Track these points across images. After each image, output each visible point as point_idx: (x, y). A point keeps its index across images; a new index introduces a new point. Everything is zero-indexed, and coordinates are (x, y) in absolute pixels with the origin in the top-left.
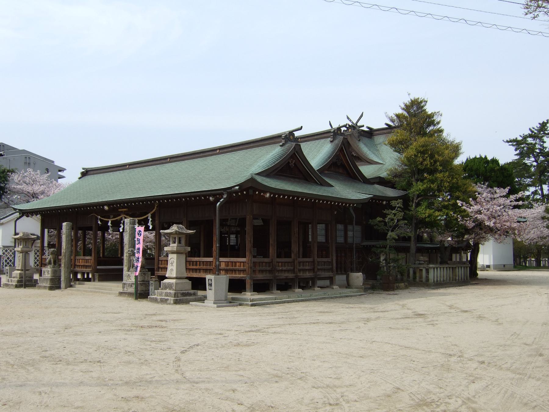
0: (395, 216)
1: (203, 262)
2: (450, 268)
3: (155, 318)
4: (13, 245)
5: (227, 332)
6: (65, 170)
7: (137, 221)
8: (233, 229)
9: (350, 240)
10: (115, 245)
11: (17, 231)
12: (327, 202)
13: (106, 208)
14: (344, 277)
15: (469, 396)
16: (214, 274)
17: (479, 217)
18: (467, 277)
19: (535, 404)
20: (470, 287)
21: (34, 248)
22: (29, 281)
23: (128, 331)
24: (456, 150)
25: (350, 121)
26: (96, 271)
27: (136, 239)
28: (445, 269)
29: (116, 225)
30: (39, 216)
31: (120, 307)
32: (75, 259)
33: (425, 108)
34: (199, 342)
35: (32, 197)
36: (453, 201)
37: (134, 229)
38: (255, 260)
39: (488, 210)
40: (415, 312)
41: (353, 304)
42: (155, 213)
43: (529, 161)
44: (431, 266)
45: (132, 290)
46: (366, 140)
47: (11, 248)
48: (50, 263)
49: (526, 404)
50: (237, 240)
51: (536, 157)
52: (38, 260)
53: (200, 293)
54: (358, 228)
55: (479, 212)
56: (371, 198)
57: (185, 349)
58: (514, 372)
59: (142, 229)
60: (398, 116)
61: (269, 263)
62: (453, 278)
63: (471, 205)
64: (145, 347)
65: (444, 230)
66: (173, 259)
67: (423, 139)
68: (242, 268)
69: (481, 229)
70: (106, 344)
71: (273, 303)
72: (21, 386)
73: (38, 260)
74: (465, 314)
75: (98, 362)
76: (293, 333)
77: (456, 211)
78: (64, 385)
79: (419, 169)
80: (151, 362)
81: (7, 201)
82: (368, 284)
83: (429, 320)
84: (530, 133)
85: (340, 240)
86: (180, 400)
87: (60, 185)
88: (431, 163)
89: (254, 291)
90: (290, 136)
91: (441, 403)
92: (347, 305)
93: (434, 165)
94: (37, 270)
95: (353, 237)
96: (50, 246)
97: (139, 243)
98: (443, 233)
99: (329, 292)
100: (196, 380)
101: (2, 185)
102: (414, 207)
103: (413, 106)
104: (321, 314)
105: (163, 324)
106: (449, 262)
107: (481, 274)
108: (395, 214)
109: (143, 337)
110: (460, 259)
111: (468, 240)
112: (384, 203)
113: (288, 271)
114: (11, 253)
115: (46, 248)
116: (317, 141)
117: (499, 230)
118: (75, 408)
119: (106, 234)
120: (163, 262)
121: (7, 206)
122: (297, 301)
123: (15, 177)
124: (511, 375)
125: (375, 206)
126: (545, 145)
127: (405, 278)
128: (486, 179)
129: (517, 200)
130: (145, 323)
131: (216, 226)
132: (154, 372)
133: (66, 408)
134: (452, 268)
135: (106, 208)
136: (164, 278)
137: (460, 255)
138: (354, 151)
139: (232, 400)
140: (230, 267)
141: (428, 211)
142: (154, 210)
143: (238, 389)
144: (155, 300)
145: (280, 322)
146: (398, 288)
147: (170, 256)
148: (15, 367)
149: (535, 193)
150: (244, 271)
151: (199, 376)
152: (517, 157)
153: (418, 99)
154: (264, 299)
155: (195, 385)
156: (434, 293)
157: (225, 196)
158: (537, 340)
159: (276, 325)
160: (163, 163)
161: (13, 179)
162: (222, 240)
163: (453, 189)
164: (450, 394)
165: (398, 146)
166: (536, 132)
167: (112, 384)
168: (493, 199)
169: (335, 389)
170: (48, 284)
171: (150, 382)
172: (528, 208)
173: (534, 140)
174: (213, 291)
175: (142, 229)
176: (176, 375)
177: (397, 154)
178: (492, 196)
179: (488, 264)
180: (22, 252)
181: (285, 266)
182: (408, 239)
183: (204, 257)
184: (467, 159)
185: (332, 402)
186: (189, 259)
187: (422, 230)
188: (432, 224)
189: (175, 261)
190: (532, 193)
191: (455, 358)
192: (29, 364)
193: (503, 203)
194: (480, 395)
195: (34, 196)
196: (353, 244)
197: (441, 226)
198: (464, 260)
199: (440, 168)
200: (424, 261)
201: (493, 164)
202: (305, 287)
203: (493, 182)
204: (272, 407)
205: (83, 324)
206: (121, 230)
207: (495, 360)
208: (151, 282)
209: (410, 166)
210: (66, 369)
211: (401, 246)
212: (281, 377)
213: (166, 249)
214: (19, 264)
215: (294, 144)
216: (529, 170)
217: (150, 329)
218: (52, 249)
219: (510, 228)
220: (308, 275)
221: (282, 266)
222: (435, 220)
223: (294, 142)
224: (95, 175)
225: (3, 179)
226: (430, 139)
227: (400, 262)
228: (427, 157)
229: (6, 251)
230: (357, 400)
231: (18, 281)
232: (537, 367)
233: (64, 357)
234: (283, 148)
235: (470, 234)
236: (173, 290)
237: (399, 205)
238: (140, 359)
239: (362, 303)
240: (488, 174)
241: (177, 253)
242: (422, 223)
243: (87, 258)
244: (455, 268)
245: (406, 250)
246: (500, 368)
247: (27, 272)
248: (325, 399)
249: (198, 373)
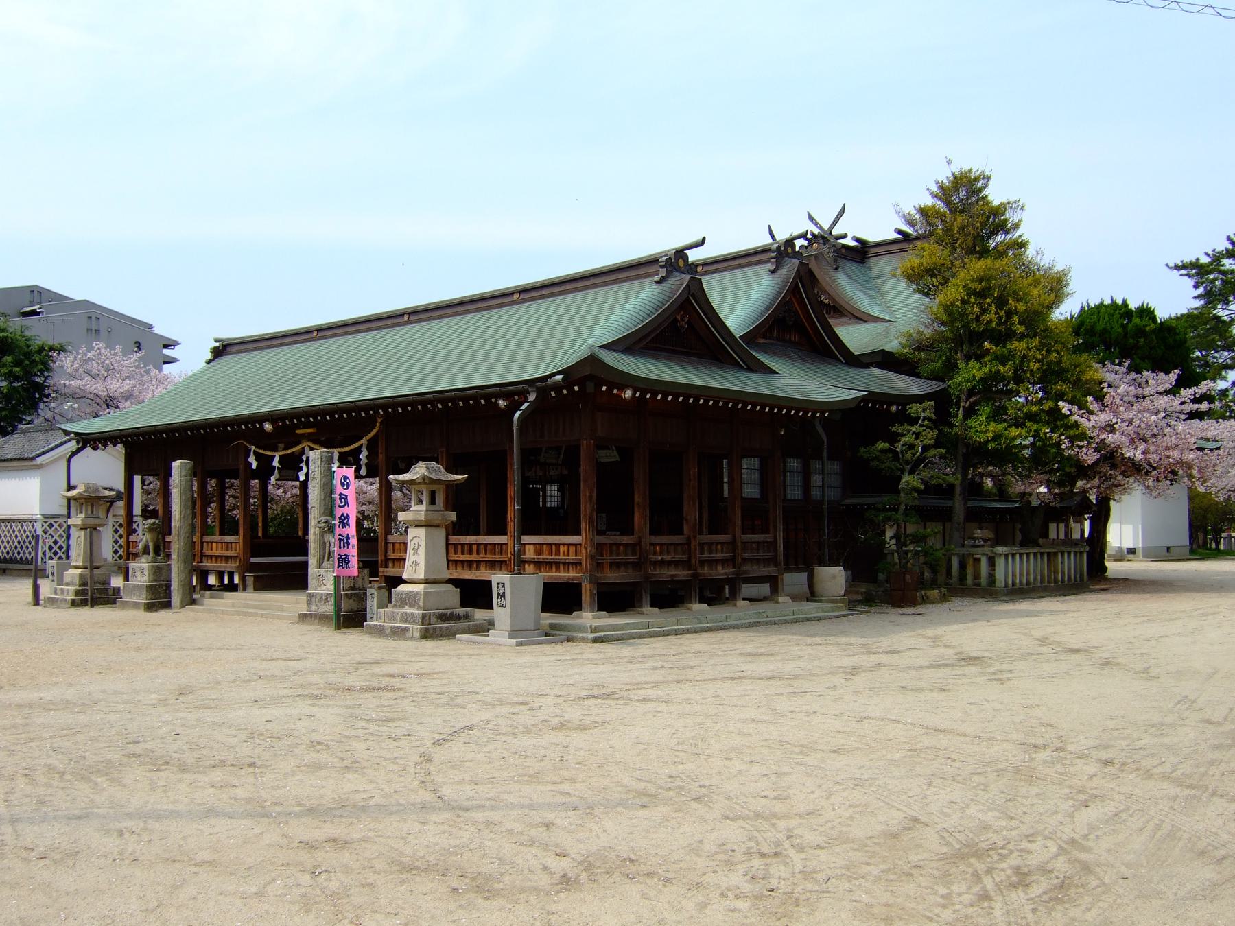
0: (916, 438)
1: (486, 545)
2: (1042, 554)
3: (378, 670)
4: (65, 512)
6: (178, 343)
7: (336, 456)
8: (552, 472)
9: (815, 494)
10: (291, 511)
11: (72, 483)
12: (763, 407)
13: (268, 427)
14: (804, 575)
15: (1076, 836)
16: (510, 571)
17: (1111, 439)
18: (1081, 575)
19: (1223, 852)
20: (1088, 596)
21: (111, 520)
22: (100, 591)
23: (318, 697)
24: (1056, 286)
25: (816, 224)
26: (248, 567)
27: (336, 496)
28: (1032, 557)
29: (292, 465)
30: (120, 447)
31: (302, 647)
32: (202, 543)
33: (986, 192)
34: (475, 721)
37: (330, 474)
38: (603, 539)
39: (1130, 422)
40: (961, 653)
41: (822, 635)
42: (376, 436)
43: (1228, 312)
44: (1000, 550)
45: (328, 609)
46: (851, 267)
47: (61, 520)
48: (146, 551)
49: (1202, 853)
50: (562, 496)
52: (121, 546)
53: (480, 614)
54: (834, 467)
55: (1110, 428)
56: (863, 399)
57: (442, 736)
58: (1178, 783)
59: (350, 472)
60: (923, 212)
61: (634, 545)
62: (1049, 577)
64: (353, 732)
65: (1030, 471)
66: (417, 539)
67: (980, 263)
68: (572, 557)
69: (1114, 466)
70: (269, 726)
71: (641, 636)
72: (79, 817)
73: (121, 546)
76: (687, 700)
77: (1056, 426)
79: (972, 332)
80: (365, 764)
81: (49, 415)
82: (857, 593)
83: (992, 670)
85: (794, 493)
86: (427, 847)
87: (166, 378)
88: (999, 318)
89: (599, 609)
91: (1011, 852)
92: (808, 640)
93: (1006, 322)
94: (120, 568)
95: (823, 486)
96: (147, 513)
97: (347, 503)
98: (1028, 477)
99: (768, 609)
100: (465, 803)
101: (38, 380)
102: (960, 417)
104: (749, 659)
105: (397, 682)
106: (1041, 541)
108: (917, 435)
109: (350, 710)
110: (1066, 534)
111: (1084, 492)
112: (894, 409)
113: (676, 563)
114: (61, 531)
116: (740, 272)
117: (1154, 469)
118: (196, 865)
120: (397, 546)
121: (50, 425)
123: (66, 363)
124: (1172, 790)
125: (873, 415)
127: (941, 578)
128: (1125, 354)
129: (1196, 401)
130: (357, 680)
131: (512, 464)
132: (373, 786)
133: (177, 865)
134: (1049, 554)
135: (268, 427)
136: (399, 581)
137: (1067, 527)
138: (825, 292)
139: (544, 846)
140: (545, 556)
141: (994, 428)
142: (373, 433)
143: (558, 821)
144: (380, 632)
145: (657, 676)
146: (925, 600)
147: (412, 532)
148: (68, 777)
150: (576, 564)
151: (472, 794)
152: (1198, 303)
153: (970, 171)
155: (461, 813)
157: (532, 397)
159: (646, 683)
160: (393, 326)
161: (62, 367)
162: (529, 497)
163: (1050, 376)
164: (1031, 831)
165: (926, 279)
167: (279, 814)
168: (1141, 398)
169: (774, 821)
170: (143, 598)
171: (364, 809)
172: (1224, 418)
176: (422, 792)
177: (923, 297)
178: (1140, 391)
179: (1131, 545)
180: (83, 528)
181: (668, 553)
182: (949, 490)
183: (489, 533)
184: (1083, 308)
185: (765, 849)
186: (454, 539)
187: (981, 470)
188: (1003, 455)
189: (423, 544)
191: (1048, 753)
193: (1163, 406)
195: (110, 403)
196: (822, 502)
197: (1023, 461)
198: (1076, 536)
199: (1021, 329)
201: (1141, 317)
203: (1142, 359)
204: (632, 861)
205: (218, 683)
206: (302, 478)
207: (1137, 757)
208: (370, 591)
210: (179, 781)
212: (654, 796)
213: (401, 516)
214: (78, 554)
215: (687, 277)
217: (366, 695)
218: (151, 521)
219: (1180, 463)
220: (721, 572)
221: (661, 553)
226: (998, 263)
227: (930, 542)
228: (989, 305)
229: (51, 526)
230: (823, 845)
231: (77, 593)
233: (175, 755)
234: (661, 287)
235: (1089, 478)
236: (419, 607)
237: (927, 413)
239: (843, 633)
240: (1131, 341)
241: (427, 525)
242: (978, 454)
243: (228, 538)
244: (1055, 554)
245: (944, 515)
246: (1149, 775)
247: (96, 572)
248: (752, 844)
249: (469, 788)
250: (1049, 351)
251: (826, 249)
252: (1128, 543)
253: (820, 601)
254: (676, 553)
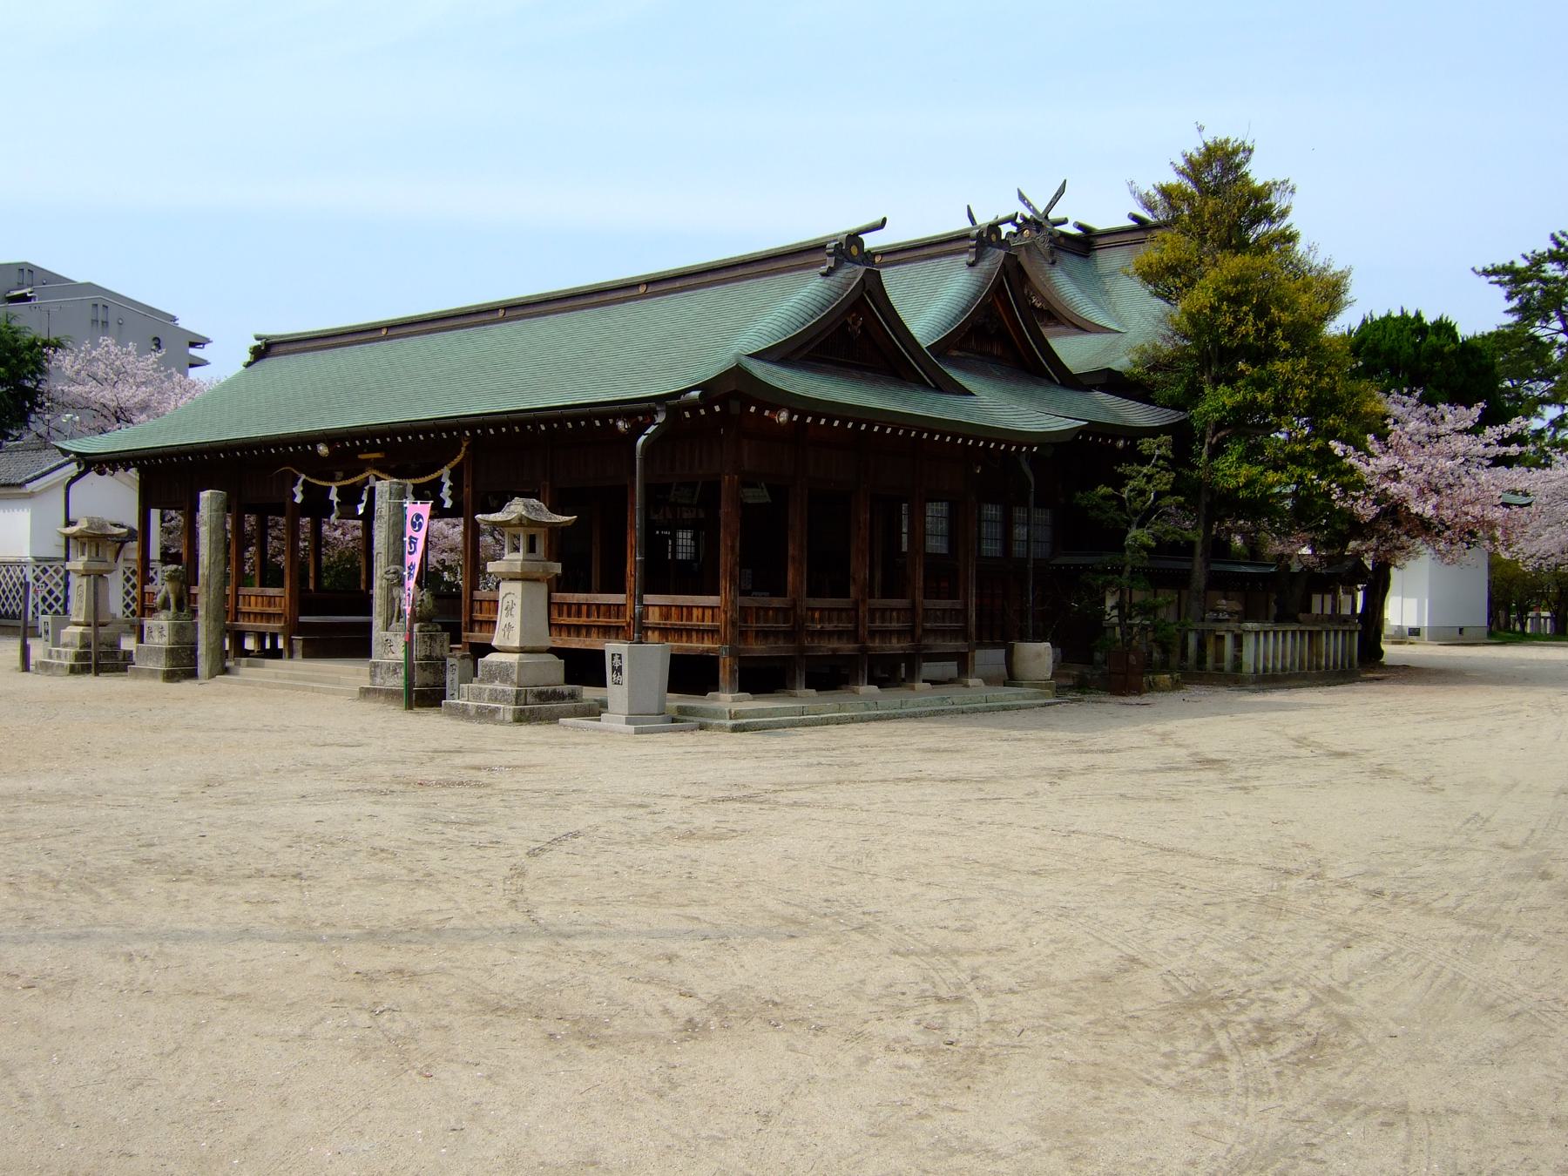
0: (1148, 482)
2: (1302, 633)
3: (458, 760)
5: (659, 801)
6: (207, 341)
7: (410, 488)
8: (685, 516)
9: (1018, 550)
10: (352, 559)
13: (323, 449)
14: (1000, 654)
15: (1334, 984)
16: (628, 639)
17: (1393, 488)
19: (1516, 1007)
20: (1358, 687)
21: (121, 565)
24: (1332, 293)
25: (1029, 205)
26: (295, 628)
28: (1289, 636)
30: (133, 473)
31: (363, 730)
32: (237, 597)
33: (1245, 169)
34: (581, 826)
35: (114, 419)
36: (1319, 442)
37: (401, 509)
38: (747, 601)
39: (1420, 468)
40: (1196, 754)
41: (1022, 728)
42: (460, 464)
43: (1547, 332)
44: (1250, 625)
45: (397, 682)
46: (1071, 261)
47: (57, 564)
48: (165, 605)
49: (1491, 1007)
50: (697, 547)
52: (134, 599)
53: (589, 693)
56: (1081, 430)
58: (1463, 920)
59: (425, 509)
60: (1166, 192)
61: (785, 610)
62: (1310, 661)
63: (1371, 455)
64: (426, 838)
65: (1291, 528)
68: (708, 623)
69: (1397, 524)
70: (320, 828)
71: (793, 725)
72: (77, 937)
73: (134, 599)
74: (1339, 763)
75: (295, 877)
78: (197, 936)
79: (1222, 348)
80: (441, 877)
81: (42, 430)
82: (1068, 676)
83: (1235, 776)
84: (1554, 248)
86: (518, 981)
87: (193, 385)
88: (1258, 331)
89: (741, 690)
90: (849, 245)
91: (1252, 1002)
92: (1004, 733)
93: (1266, 336)
94: (132, 626)
98: (1288, 534)
99: (954, 694)
100: (567, 929)
102: (1205, 456)
103: (1209, 164)
104: (929, 756)
105: (483, 776)
106: (1301, 616)
107: (1391, 652)
108: (1149, 478)
110: (1333, 609)
111: (1358, 555)
112: (1121, 444)
113: (840, 634)
114: (57, 578)
115: (156, 565)
116: (930, 264)
117: (1448, 528)
118: (225, 999)
119: (325, 527)
120: (485, 605)
121: (44, 443)
122: (862, 720)
123: (64, 363)
124: (1457, 930)
125: (1095, 451)
127: (1174, 660)
128: (1415, 380)
129: (1504, 442)
130: (430, 773)
131: (633, 504)
132: (451, 904)
133: (201, 999)
134: (1311, 632)
135: (323, 449)
136: (488, 649)
137: (1335, 599)
138: (1037, 293)
139: (664, 983)
140: (674, 622)
141: (1246, 471)
142: (459, 457)
143: (681, 953)
144: (462, 713)
145: (812, 775)
146: (1153, 688)
147: (505, 587)
148: (63, 886)
150: (713, 632)
151: (575, 917)
152: (1511, 319)
153: (1227, 141)
154: (770, 713)
155: (562, 941)
156: (1254, 704)
157: (660, 419)
158: (1537, 835)
160: (484, 323)
162: (655, 548)
163: (1320, 406)
164: (1278, 977)
165: (1166, 279)
167: (331, 937)
169: (955, 958)
170: (162, 665)
171: (438, 933)
172: (1538, 466)
174: (625, 688)
175: (425, 509)
176: (512, 913)
177: (1162, 302)
178: (1433, 428)
179: (1414, 624)
180: (86, 574)
184: (1364, 321)
185: (943, 993)
186: (558, 597)
187: (1228, 524)
188: (1258, 506)
189: (518, 602)
190: (1552, 423)
191: (1302, 880)
192: (103, 880)
193: (1462, 450)
194: (1362, 980)
195: (121, 416)
197: (1280, 513)
198: (1346, 611)
199: (1285, 346)
200: (1230, 614)
201: (1438, 335)
202: (887, 680)
203: (1438, 388)
204: (775, 1004)
205: (257, 773)
207: (1413, 887)
208: (450, 661)
209: (1197, 337)
210: (205, 894)
212: (806, 924)
213: (492, 567)
214: (78, 607)
216: (1546, 355)
219: (1482, 522)
220: (896, 646)
221: (821, 620)
222: (1265, 497)
223: (861, 263)
224: (292, 357)
225: (32, 367)
226: (1259, 261)
227: (1162, 614)
228: (1246, 314)
229: (45, 571)
231: (78, 656)
232: (1531, 909)
233: (200, 862)
234: (828, 281)
236: (512, 682)
237: (1163, 450)
238: (412, 871)
241: (524, 578)
242: (1226, 504)
243: (271, 591)
244: (1320, 632)
245: (1180, 581)
246: (1428, 910)
247: (102, 630)
248: (927, 986)
249: (572, 909)
250: (1320, 376)
251: (1040, 238)
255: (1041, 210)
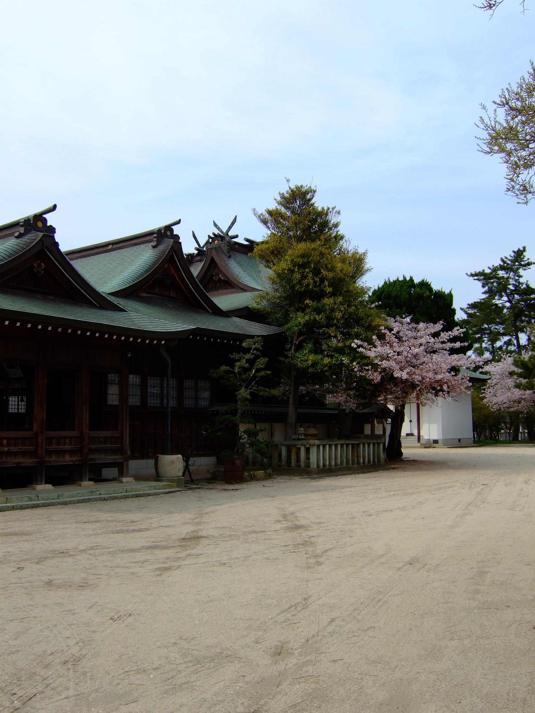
9: (153, 402)
14: (152, 461)
17: (385, 364)
24: (357, 265)
25: (219, 229)
28: (339, 447)
33: (313, 201)
43: (501, 302)
46: (241, 257)
51: (510, 295)
84: (502, 264)
88: (315, 282)
93: (320, 285)
113: (23, 454)
126: (521, 280)
134: (353, 445)
138: (222, 272)
141: (312, 357)
146: (253, 478)
149: (509, 343)
152: (484, 296)
153: (302, 186)
166: (509, 262)
173: (507, 273)
179: (436, 438)
190: (505, 343)
199: (329, 290)
201: (421, 289)
211: (267, 412)
221: (8, 445)
234: (18, 241)
237: (257, 345)
240: (414, 303)
242: (304, 376)
244: (358, 445)
250: (349, 306)
251: (223, 245)
252: (435, 436)
253: (162, 481)
254: (70, 444)
255: (225, 231)
